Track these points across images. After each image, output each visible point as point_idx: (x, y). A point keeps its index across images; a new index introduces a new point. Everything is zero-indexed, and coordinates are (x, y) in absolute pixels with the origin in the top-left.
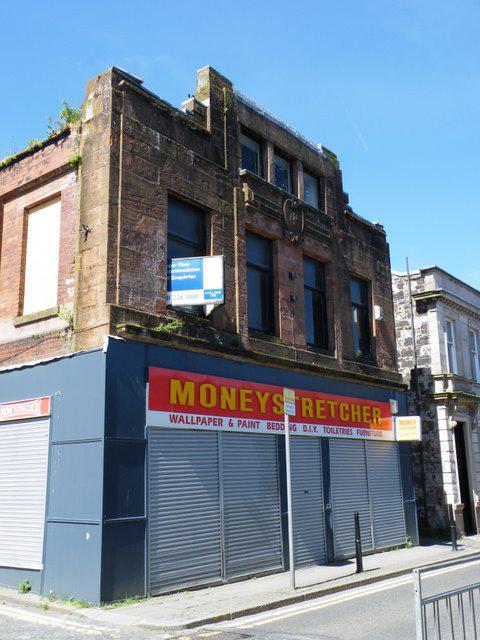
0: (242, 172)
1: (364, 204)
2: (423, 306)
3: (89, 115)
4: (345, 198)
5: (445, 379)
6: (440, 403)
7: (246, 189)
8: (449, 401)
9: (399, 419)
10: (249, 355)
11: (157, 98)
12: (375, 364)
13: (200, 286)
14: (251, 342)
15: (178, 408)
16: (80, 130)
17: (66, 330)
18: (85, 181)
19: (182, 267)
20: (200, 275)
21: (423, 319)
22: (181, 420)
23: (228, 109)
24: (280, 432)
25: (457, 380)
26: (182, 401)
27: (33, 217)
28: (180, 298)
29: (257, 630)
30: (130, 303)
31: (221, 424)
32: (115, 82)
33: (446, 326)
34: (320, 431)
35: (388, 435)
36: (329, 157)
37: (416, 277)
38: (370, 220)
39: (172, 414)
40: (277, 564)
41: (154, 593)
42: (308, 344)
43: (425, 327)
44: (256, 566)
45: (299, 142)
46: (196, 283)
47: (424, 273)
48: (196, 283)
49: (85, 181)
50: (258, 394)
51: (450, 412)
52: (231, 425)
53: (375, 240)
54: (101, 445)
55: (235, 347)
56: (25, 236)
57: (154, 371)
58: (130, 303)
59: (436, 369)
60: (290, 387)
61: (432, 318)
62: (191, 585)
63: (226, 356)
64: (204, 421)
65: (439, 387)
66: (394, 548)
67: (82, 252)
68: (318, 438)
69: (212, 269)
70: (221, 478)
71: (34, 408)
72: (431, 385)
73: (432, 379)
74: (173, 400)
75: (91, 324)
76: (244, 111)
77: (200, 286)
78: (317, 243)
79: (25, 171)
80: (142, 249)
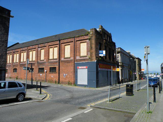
0: (104, 38)
1: (114, 40)
2: (118, 53)
3: (91, 33)
4: (112, 39)
5: (121, 63)
6: (120, 66)
7: (104, 40)
8: (121, 66)
9: (117, 68)
13: (103, 54)
16: (90, 35)
17: (89, 59)
18: (91, 41)
19: (100, 52)
20: (103, 53)
21: (118, 54)
23: (103, 30)
24: (110, 70)
25: (122, 63)
27: (81, 44)
28: (100, 55)
29: (147, 82)
32: (95, 30)
33: (121, 55)
34: (106, 70)
35: (116, 71)
36: (110, 34)
43: (118, 56)
44: (106, 85)
45: (107, 31)
46: (102, 53)
47: (118, 48)
48: (102, 53)
49: (91, 41)
51: (121, 67)
53: (114, 44)
54: (96, 72)
57: (99, 64)
59: (119, 61)
61: (119, 54)
65: (120, 64)
67: (91, 50)
69: (104, 52)
71: (85, 67)
72: (119, 63)
73: (119, 63)
75: (93, 58)
77: (103, 54)
79: (80, 38)
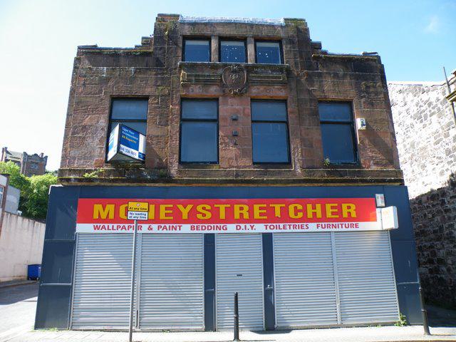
10: (182, 182)
11: (120, 49)
12: (360, 166)
14: (179, 172)
15: (100, 220)
22: (104, 227)
26: (104, 216)
30: (75, 165)
31: (284, 228)
34: (260, 228)
37: (452, 81)
38: (358, 53)
39: (95, 225)
40: (199, 325)
41: (74, 328)
42: (254, 163)
50: (180, 207)
52: (150, 228)
55: (167, 179)
56: (270, 122)
58: (75, 165)
60: (378, 193)
62: (102, 328)
63: (147, 185)
64: (124, 228)
66: (376, 325)
68: (259, 234)
70: (336, 272)
74: (96, 216)
76: (186, 27)
78: (268, 88)
80: (87, 134)
